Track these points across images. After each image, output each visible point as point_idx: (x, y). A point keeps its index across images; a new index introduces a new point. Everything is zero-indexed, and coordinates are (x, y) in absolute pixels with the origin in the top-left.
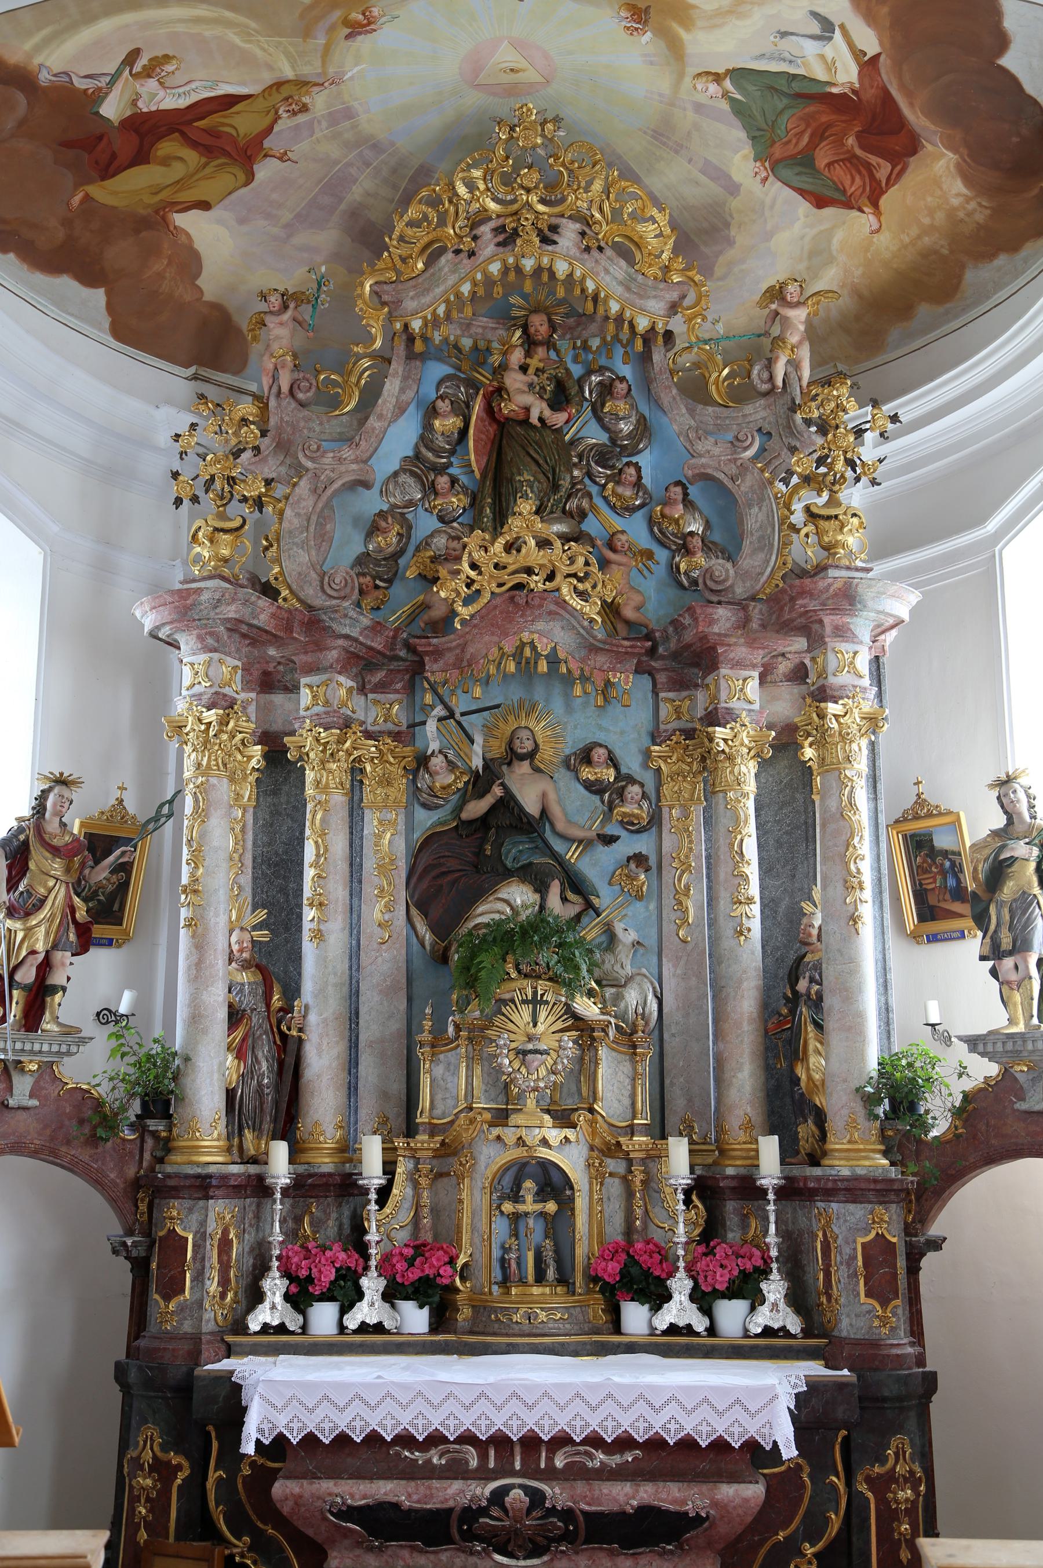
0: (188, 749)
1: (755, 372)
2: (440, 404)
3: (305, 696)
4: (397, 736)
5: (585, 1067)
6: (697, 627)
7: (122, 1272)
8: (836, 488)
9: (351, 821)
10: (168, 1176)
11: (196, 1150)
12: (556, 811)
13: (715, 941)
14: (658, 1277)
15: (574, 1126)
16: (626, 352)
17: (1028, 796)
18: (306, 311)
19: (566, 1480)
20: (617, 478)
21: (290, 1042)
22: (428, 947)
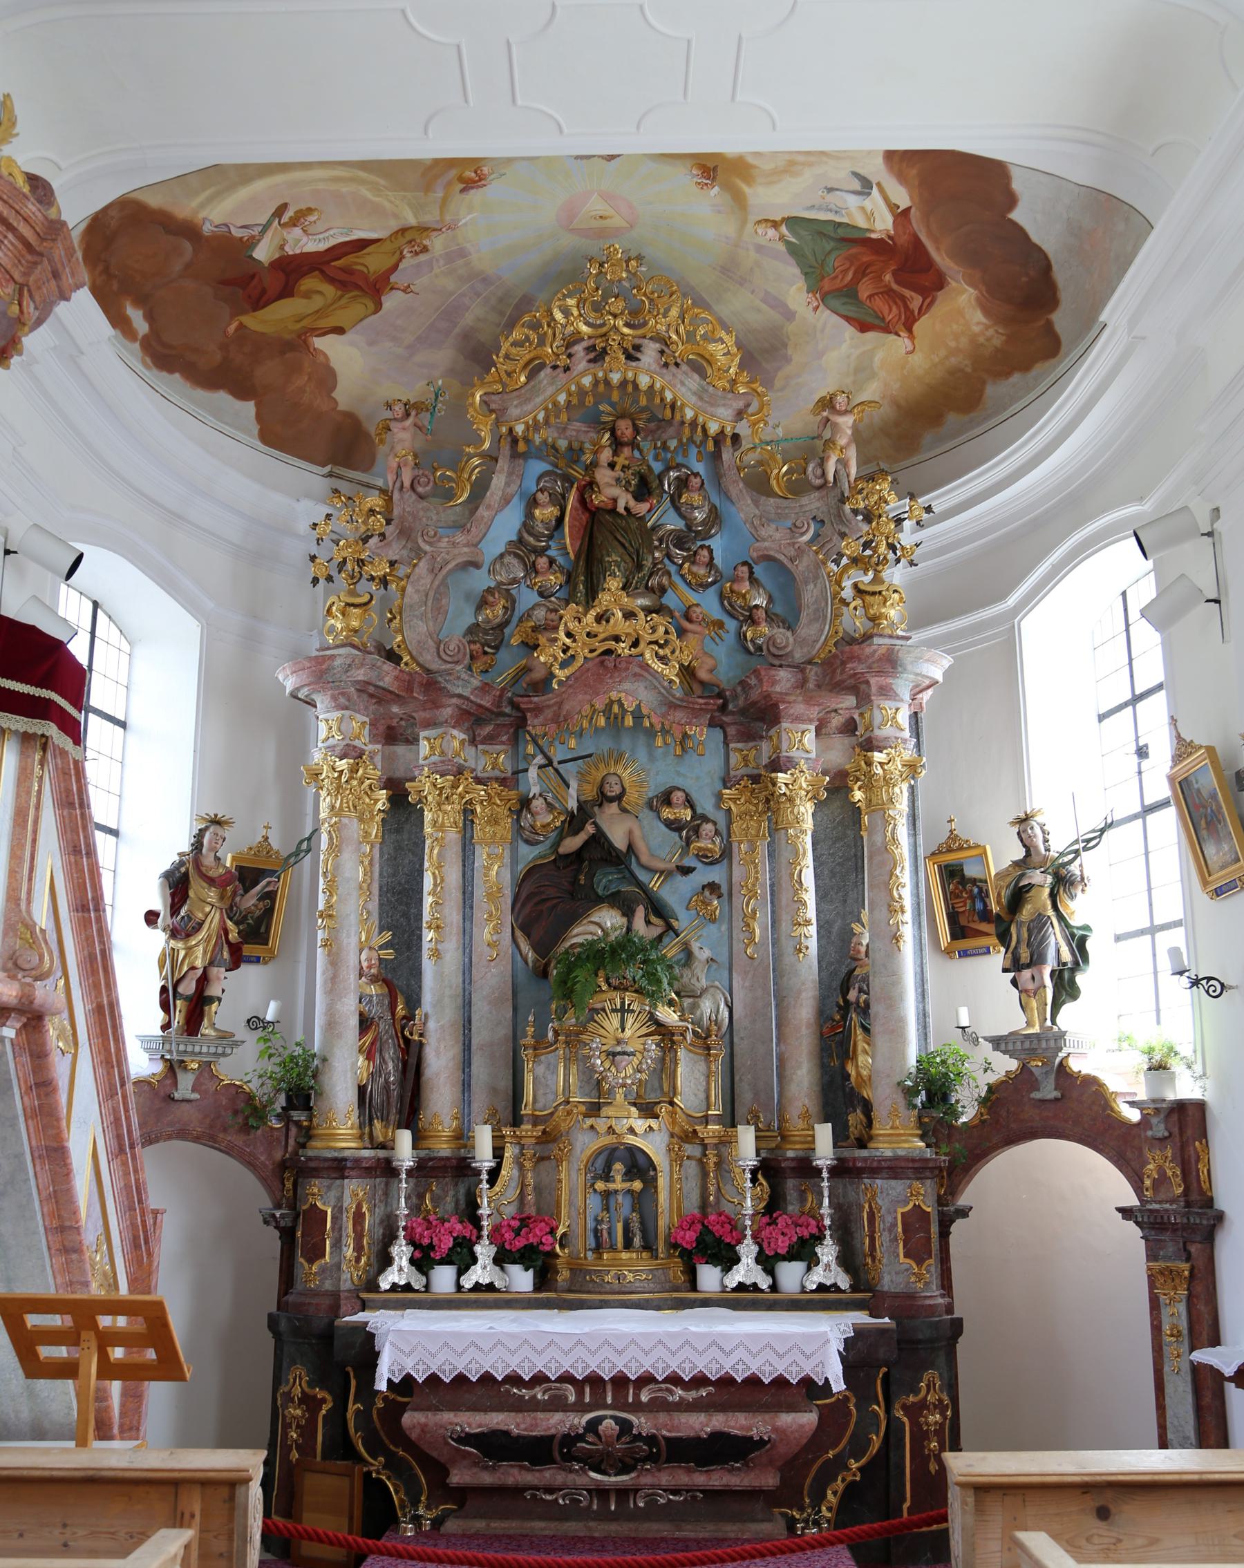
0: (323, 793)
1: (810, 469)
2: (539, 495)
3: (424, 748)
4: (503, 782)
5: (666, 1066)
6: (761, 686)
7: (272, 1241)
8: (880, 568)
9: (464, 855)
10: (310, 1159)
11: (333, 1137)
12: (640, 846)
13: (777, 958)
14: (729, 1244)
15: (657, 1117)
16: (699, 452)
17: (1043, 832)
18: (425, 418)
19: (651, 1411)
20: (692, 559)
21: (412, 1045)
22: (531, 964)
